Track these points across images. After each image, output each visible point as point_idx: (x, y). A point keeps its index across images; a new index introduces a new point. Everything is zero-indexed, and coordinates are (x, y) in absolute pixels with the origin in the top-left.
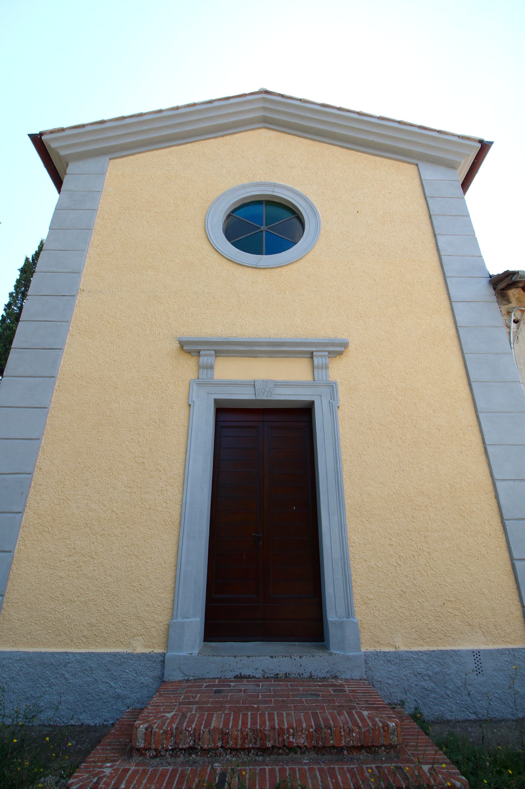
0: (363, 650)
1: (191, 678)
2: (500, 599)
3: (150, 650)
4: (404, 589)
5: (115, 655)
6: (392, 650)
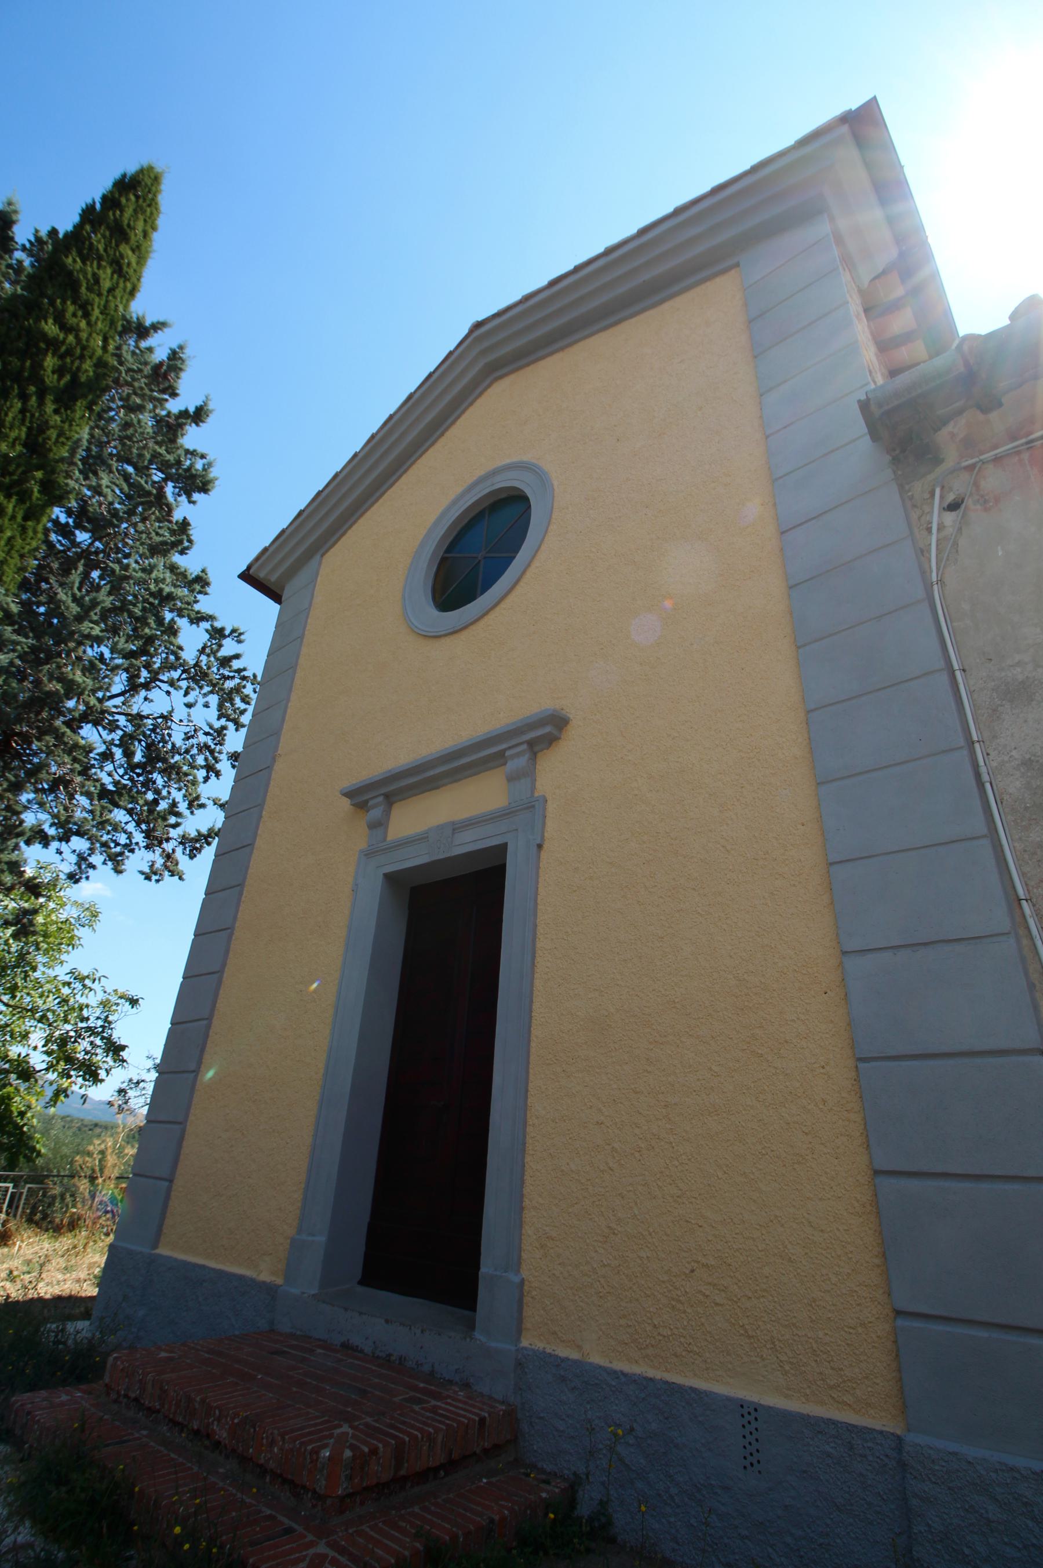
0: (525, 1343)
1: (298, 1333)
2: (834, 1279)
3: (273, 1279)
4: (613, 1225)
5: (241, 1278)
6: (574, 1355)
